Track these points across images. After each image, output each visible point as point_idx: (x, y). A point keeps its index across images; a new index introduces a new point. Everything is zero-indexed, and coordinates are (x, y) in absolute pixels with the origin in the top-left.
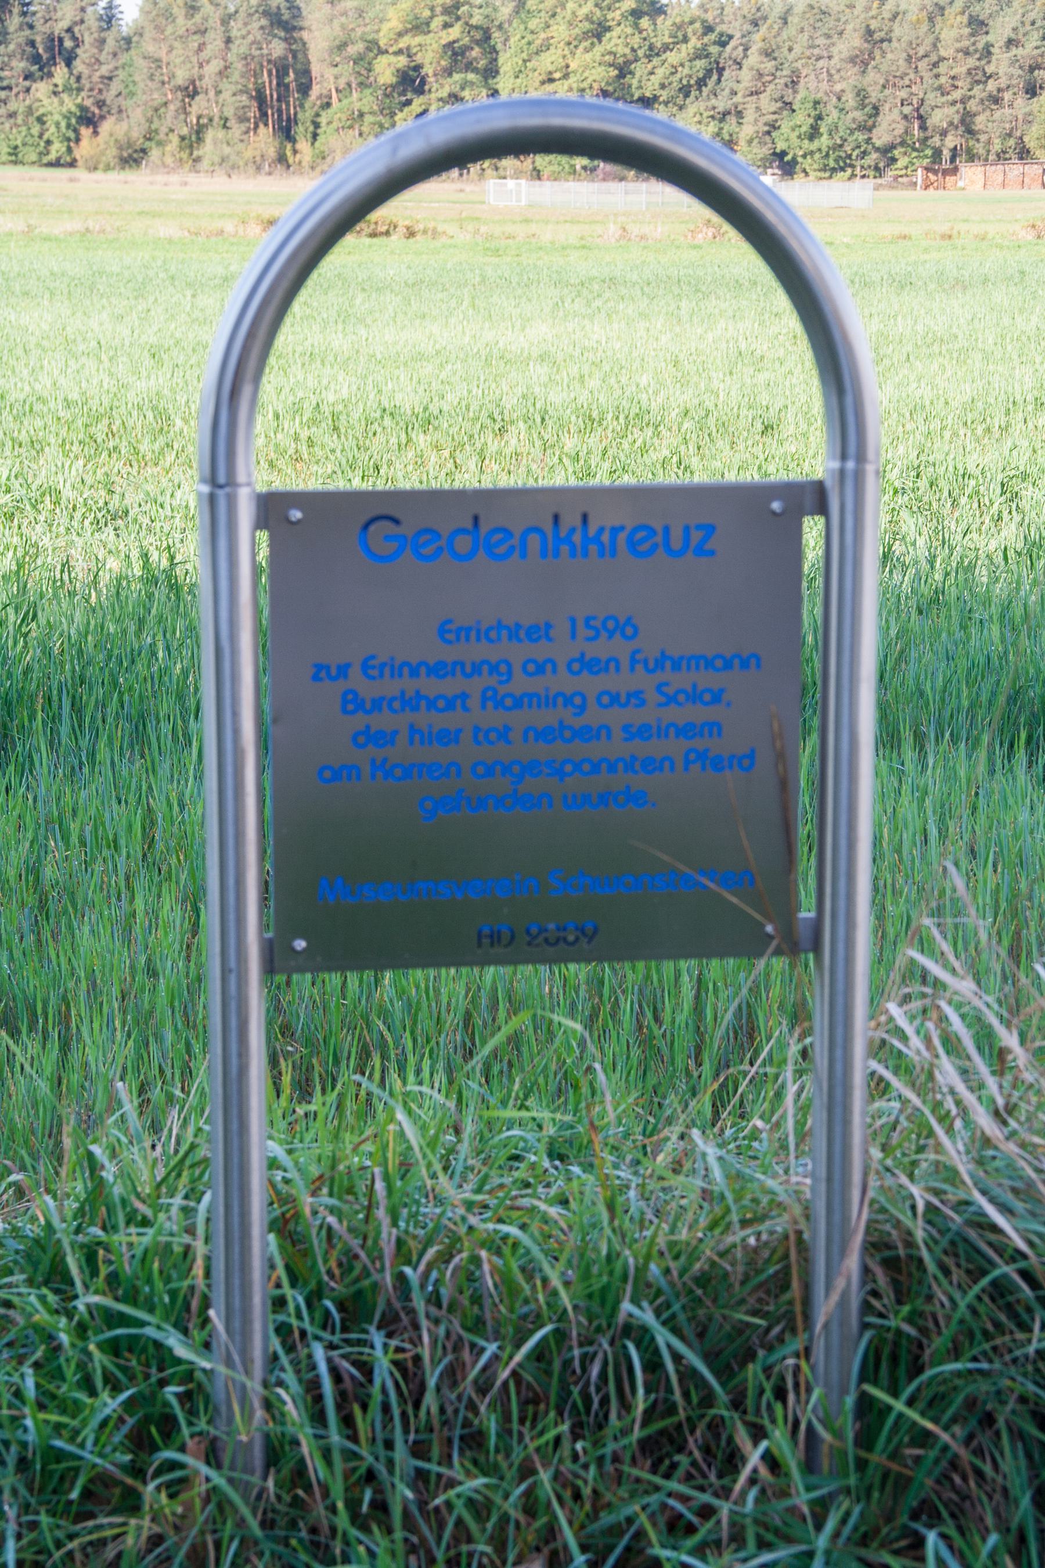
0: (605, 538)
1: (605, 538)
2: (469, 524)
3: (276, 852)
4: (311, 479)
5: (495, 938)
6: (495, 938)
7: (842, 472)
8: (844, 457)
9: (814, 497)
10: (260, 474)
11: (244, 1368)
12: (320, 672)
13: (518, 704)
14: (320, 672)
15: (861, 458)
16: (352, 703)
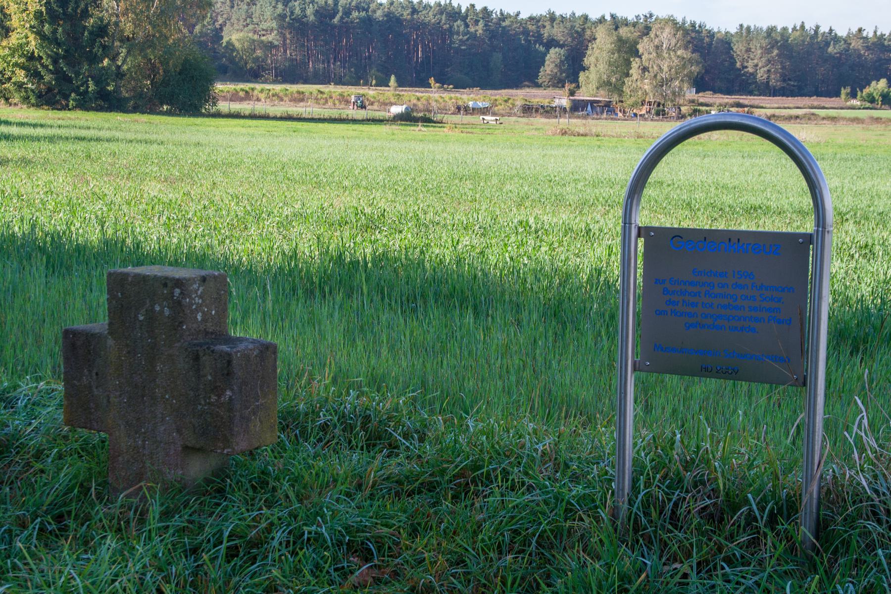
0: (745, 246)
1: (745, 246)
2: (703, 239)
3: (248, 81)
4: (667, 222)
5: (706, 369)
6: (706, 369)
7: (818, 231)
8: (818, 226)
9: (808, 238)
10: (643, 218)
11: (432, 81)
12: (657, 281)
13: (716, 297)
14: (657, 281)
15: (824, 227)
16: (666, 291)
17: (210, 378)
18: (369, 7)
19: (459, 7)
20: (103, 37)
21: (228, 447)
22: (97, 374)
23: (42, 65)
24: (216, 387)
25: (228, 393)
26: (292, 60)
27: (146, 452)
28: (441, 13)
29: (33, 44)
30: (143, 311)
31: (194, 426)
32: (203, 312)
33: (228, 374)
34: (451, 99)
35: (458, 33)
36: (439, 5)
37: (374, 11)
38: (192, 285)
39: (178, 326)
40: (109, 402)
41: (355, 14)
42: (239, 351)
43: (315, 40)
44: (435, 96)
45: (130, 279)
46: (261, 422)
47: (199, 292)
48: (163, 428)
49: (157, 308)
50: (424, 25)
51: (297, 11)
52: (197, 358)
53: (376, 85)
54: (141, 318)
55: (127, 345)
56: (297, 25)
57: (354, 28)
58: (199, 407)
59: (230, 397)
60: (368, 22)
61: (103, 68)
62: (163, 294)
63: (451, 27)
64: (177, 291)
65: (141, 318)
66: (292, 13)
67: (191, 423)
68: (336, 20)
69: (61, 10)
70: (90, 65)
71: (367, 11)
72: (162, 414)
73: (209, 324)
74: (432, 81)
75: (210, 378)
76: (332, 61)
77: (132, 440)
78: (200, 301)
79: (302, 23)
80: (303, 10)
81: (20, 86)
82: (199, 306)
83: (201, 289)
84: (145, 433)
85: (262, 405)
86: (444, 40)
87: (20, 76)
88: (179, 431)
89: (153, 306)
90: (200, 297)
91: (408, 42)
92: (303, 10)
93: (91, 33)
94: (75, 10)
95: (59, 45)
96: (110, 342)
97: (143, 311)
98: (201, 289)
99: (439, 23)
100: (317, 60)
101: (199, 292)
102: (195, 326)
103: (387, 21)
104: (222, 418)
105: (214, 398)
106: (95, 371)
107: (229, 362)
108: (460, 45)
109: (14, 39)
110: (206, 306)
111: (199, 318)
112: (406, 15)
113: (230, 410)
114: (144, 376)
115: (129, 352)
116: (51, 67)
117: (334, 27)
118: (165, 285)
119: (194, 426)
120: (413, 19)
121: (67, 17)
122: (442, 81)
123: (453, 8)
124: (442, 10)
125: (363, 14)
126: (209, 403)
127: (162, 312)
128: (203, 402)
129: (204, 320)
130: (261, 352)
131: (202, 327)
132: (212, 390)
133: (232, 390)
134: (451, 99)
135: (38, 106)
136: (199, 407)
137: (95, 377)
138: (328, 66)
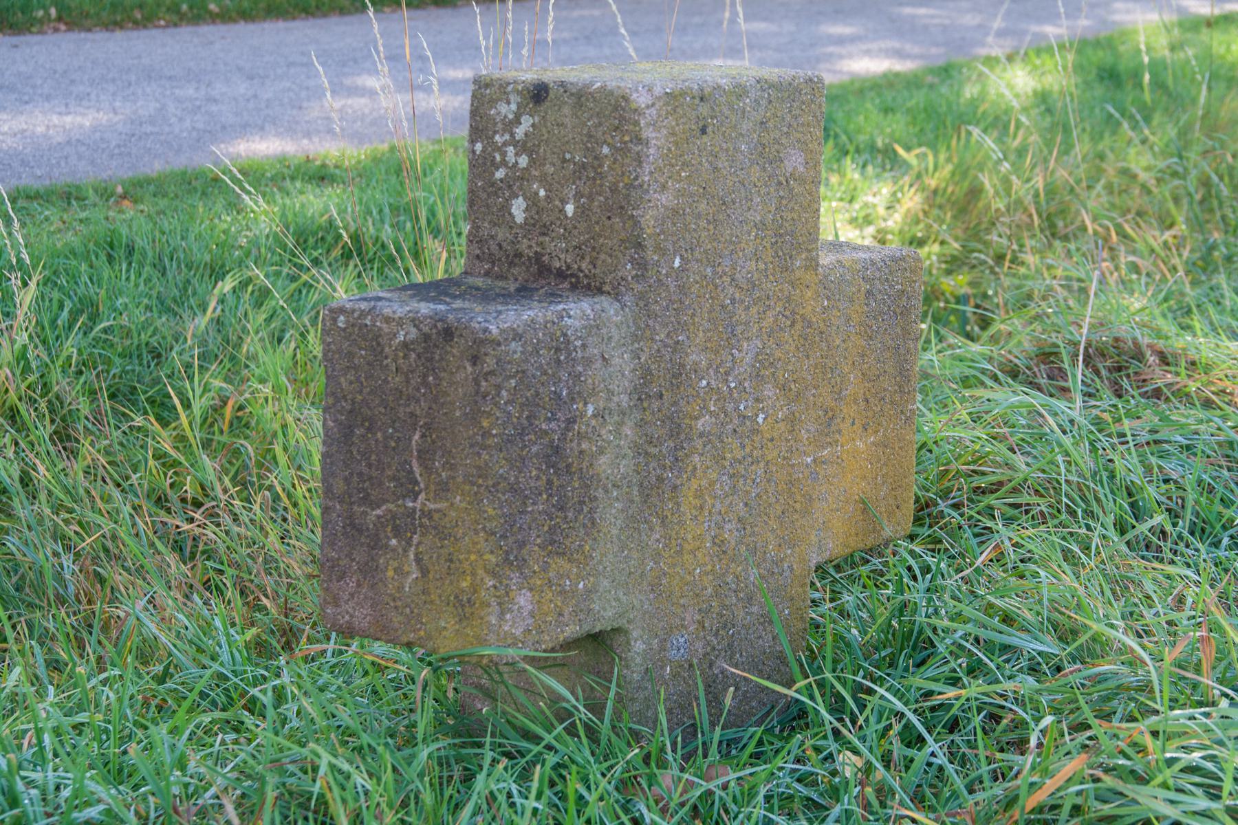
32: (532, 201)
46: (424, 572)
47: (520, 132)
78: (523, 161)
83: (527, 122)
85: (429, 514)
90: (522, 147)
98: (527, 122)
101: (520, 132)
110: (543, 180)
111: (518, 209)
130: (426, 337)
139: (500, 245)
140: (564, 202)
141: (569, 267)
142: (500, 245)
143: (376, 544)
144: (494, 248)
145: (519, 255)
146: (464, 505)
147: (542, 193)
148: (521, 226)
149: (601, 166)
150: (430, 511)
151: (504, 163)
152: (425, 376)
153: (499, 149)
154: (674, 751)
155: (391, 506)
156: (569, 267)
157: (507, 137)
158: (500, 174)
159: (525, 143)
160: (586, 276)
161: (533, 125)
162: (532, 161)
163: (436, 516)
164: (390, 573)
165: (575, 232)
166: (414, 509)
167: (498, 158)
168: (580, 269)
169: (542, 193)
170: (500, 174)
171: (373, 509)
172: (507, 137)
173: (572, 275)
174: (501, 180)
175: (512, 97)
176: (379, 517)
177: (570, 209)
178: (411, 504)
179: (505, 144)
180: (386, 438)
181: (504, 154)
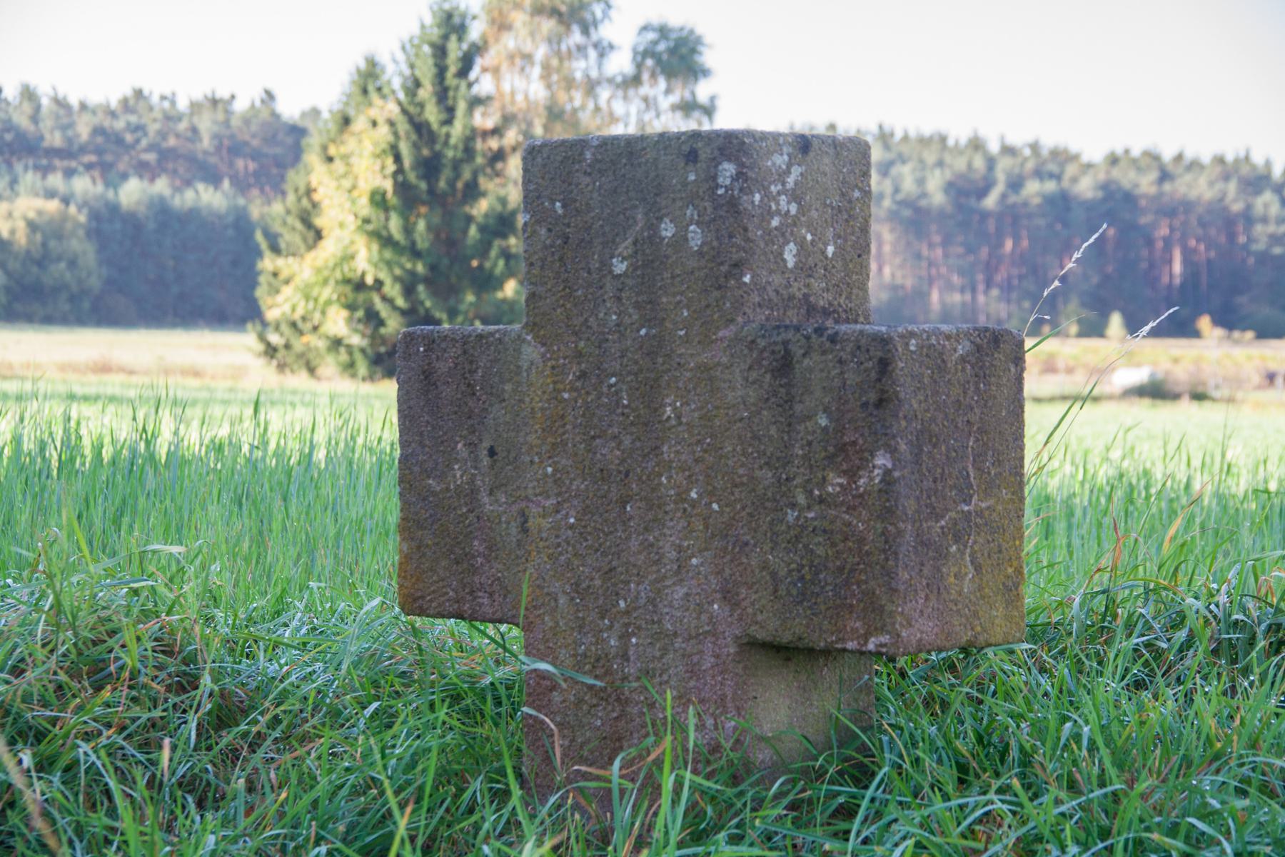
11: (1204, 323)
17: (823, 421)
18: (1062, 173)
19: (1268, 164)
20: (504, 236)
21: (882, 630)
22: (492, 452)
23: (385, 299)
24: (842, 448)
25: (882, 460)
26: (894, 288)
27: (631, 670)
28: (1226, 177)
29: (366, 261)
30: (625, 247)
31: (774, 575)
32: (801, 244)
33: (880, 403)
34: (1250, 358)
35: (1265, 220)
36: (1220, 160)
37: (1075, 180)
38: (770, 153)
39: (727, 276)
40: (525, 530)
41: (1033, 188)
42: (912, 334)
43: (946, 242)
44: (1212, 351)
45: (588, 155)
46: (978, 568)
47: (791, 181)
48: (680, 592)
49: (667, 230)
50: (1187, 206)
51: (909, 185)
52: (784, 365)
53: (1081, 335)
54: (620, 267)
55: (579, 355)
56: (907, 213)
57: (1030, 216)
58: (791, 515)
59: (887, 472)
60: (1061, 203)
61: (504, 301)
62: (685, 184)
63: (1249, 207)
64: (728, 169)
65: (620, 267)
66: (897, 190)
67: (765, 566)
68: (991, 201)
69: (423, 185)
70: (478, 295)
71: (1058, 177)
72: (680, 549)
73: (818, 285)
74: (1204, 323)
75: (823, 421)
76: (981, 287)
77: (590, 638)
78: (793, 209)
79: (917, 210)
80: (921, 182)
81: (336, 343)
82: (791, 224)
83: (796, 171)
84: (627, 612)
85: (980, 514)
86: (1232, 237)
87: (337, 323)
88: (728, 595)
89: (653, 228)
90: (795, 196)
91: (1150, 242)
92: (921, 182)
93: (483, 229)
94: (452, 184)
95: (416, 254)
96: (531, 352)
97: (625, 247)
98: (796, 171)
99: (1221, 200)
100: (949, 287)
101: (791, 181)
102: (777, 279)
103: (1105, 200)
104: (862, 541)
105: (836, 481)
106: (486, 444)
107: (884, 365)
108: (1270, 246)
109: (328, 249)
110: (810, 227)
111: (790, 255)
112: (1146, 184)
113: (887, 513)
114: (627, 441)
115: (583, 375)
116: (400, 302)
117: (985, 215)
118: (692, 157)
119: (774, 575)
120: (1161, 194)
121: (435, 198)
122: (1229, 320)
123: (1254, 167)
124: (1225, 169)
125: (1050, 186)
126: (821, 501)
127: (680, 240)
128: (801, 499)
129: (805, 269)
130: (979, 348)
131: (797, 289)
132: (830, 458)
133: (893, 451)
134: (1250, 358)
135: (371, 378)
136: (791, 515)
137: (486, 461)
138: (974, 298)
139: (777, 292)
140: (826, 245)
141: (830, 304)
142: (777, 292)
143: (942, 555)
144: (772, 295)
145: (791, 298)
146: (1009, 496)
147: (809, 237)
148: (791, 271)
149: (853, 209)
150: (982, 511)
151: (778, 212)
152: (977, 384)
153: (774, 199)
154: (675, 802)
155: (953, 514)
156: (830, 304)
157: (780, 187)
158: (775, 222)
159: (794, 190)
160: (845, 311)
161: (802, 174)
162: (801, 208)
163: (986, 514)
164: (952, 579)
165: (834, 271)
166: (969, 512)
167: (774, 207)
168: (840, 305)
169: (809, 237)
170: (775, 222)
171: (937, 522)
172: (780, 187)
173: (834, 311)
174: (776, 228)
175: (785, 149)
176: (942, 528)
177: (830, 250)
178: (966, 508)
179: (779, 193)
180: (948, 450)
181: (778, 204)
